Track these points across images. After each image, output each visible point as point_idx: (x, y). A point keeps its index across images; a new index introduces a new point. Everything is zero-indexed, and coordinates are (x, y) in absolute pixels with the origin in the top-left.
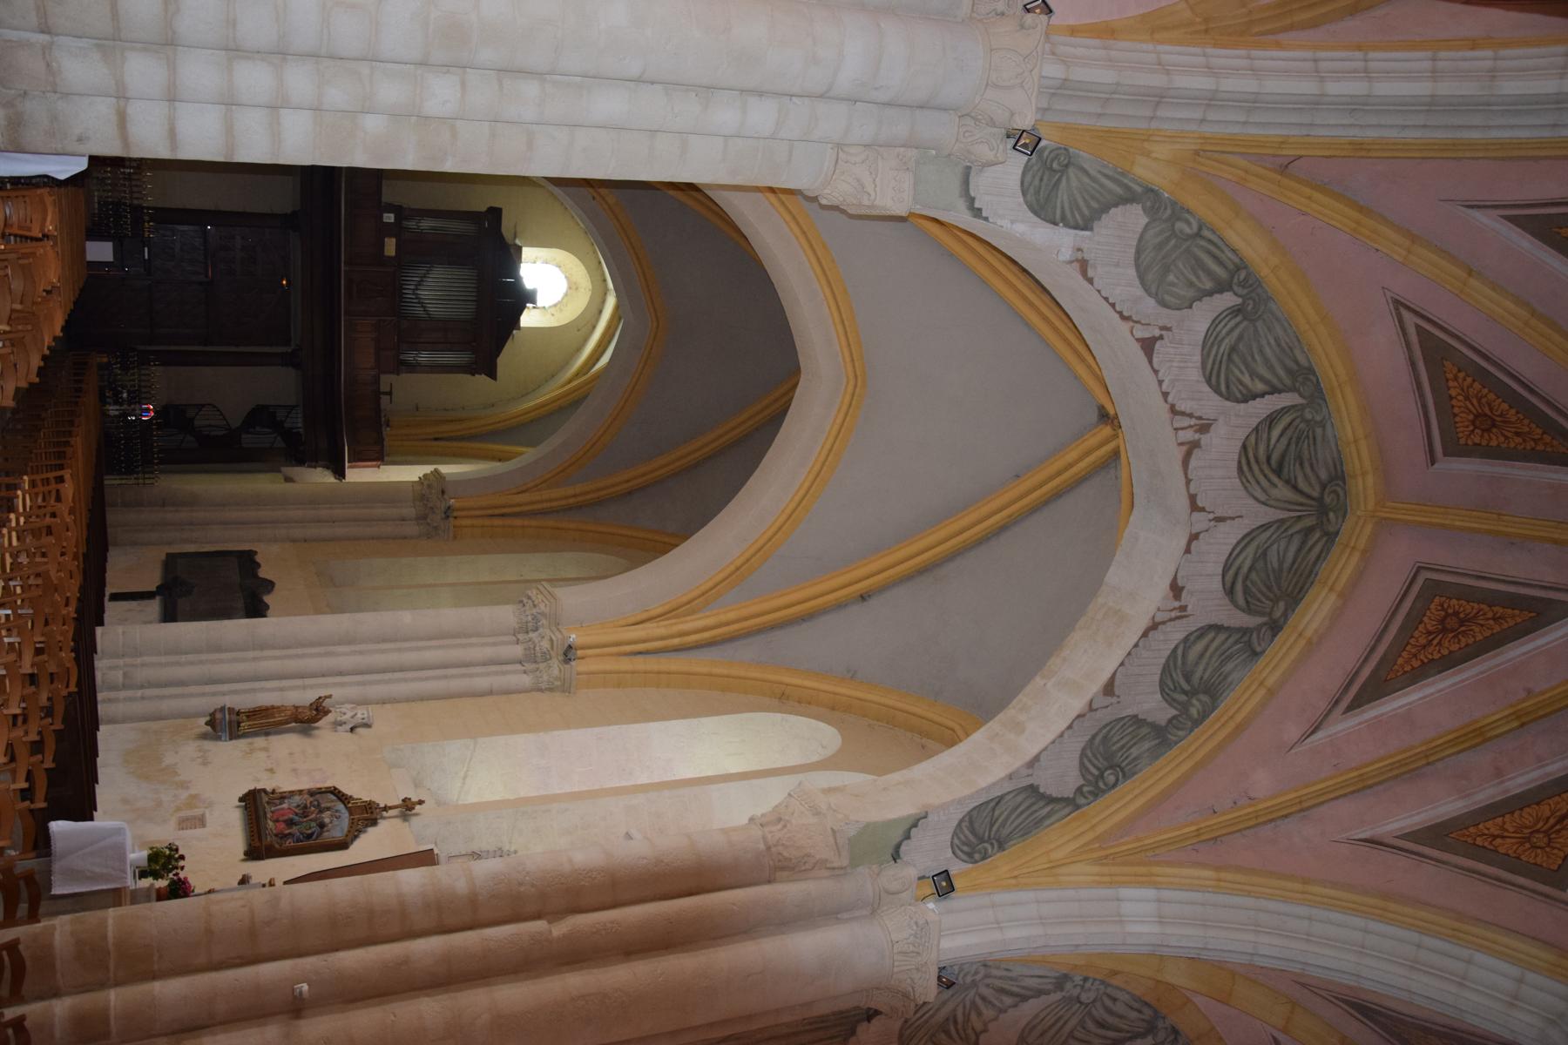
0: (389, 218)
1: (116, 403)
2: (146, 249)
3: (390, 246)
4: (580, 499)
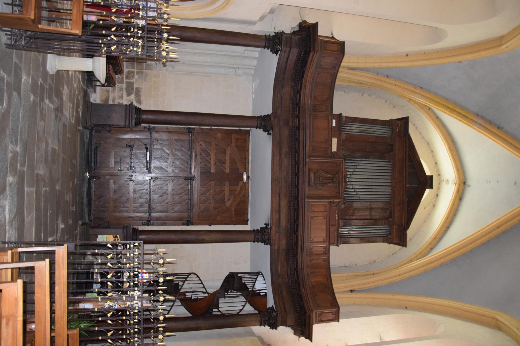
2: (148, 153)
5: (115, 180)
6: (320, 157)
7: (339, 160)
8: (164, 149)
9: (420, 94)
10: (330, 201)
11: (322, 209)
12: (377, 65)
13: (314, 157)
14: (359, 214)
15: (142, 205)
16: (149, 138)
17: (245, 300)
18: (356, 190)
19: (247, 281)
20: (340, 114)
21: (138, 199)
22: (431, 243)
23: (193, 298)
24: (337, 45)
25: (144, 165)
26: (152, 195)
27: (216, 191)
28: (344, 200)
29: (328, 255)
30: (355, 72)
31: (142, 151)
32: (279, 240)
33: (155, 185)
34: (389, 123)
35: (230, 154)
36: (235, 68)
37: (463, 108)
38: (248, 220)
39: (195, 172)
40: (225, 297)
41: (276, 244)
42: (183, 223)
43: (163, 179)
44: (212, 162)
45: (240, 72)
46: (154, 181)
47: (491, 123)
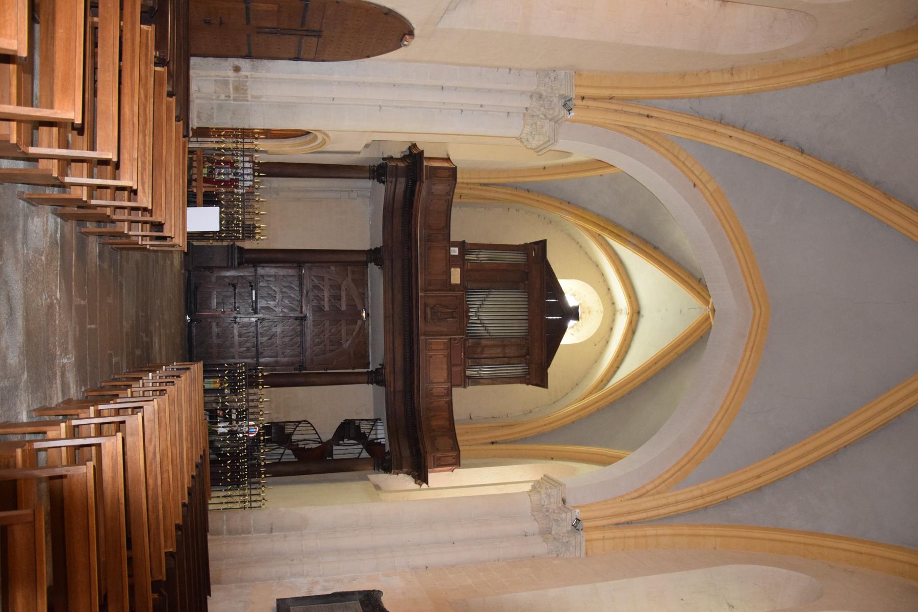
0: (454, 251)
1: (225, 420)
2: (254, 292)
3: (456, 276)
4: (708, 499)
5: (217, 323)
6: (439, 290)
7: (459, 293)
8: (271, 286)
9: (567, 211)
10: (451, 338)
11: (442, 347)
12: (512, 180)
13: (430, 291)
14: (488, 352)
15: (248, 349)
16: (254, 274)
17: (362, 447)
18: (485, 325)
19: (365, 428)
20: (464, 242)
21: (244, 344)
22: (597, 387)
23: (306, 448)
24: (447, 171)
25: (249, 305)
26: (259, 338)
27: (332, 331)
28: (467, 336)
29: (450, 398)
30: (488, 188)
31: (246, 290)
32: (394, 382)
33: (262, 327)
34: (524, 248)
35: (346, 289)
36: (349, 191)
37: (617, 225)
38: (369, 363)
39: (307, 311)
40: (339, 445)
41: (392, 386)
42: (295, 368)
43: (271, 320)
44: (326, 299)
45: (354, 195)
46: (260, 323)
47: (647, 242)
